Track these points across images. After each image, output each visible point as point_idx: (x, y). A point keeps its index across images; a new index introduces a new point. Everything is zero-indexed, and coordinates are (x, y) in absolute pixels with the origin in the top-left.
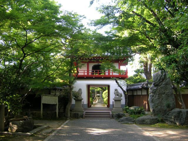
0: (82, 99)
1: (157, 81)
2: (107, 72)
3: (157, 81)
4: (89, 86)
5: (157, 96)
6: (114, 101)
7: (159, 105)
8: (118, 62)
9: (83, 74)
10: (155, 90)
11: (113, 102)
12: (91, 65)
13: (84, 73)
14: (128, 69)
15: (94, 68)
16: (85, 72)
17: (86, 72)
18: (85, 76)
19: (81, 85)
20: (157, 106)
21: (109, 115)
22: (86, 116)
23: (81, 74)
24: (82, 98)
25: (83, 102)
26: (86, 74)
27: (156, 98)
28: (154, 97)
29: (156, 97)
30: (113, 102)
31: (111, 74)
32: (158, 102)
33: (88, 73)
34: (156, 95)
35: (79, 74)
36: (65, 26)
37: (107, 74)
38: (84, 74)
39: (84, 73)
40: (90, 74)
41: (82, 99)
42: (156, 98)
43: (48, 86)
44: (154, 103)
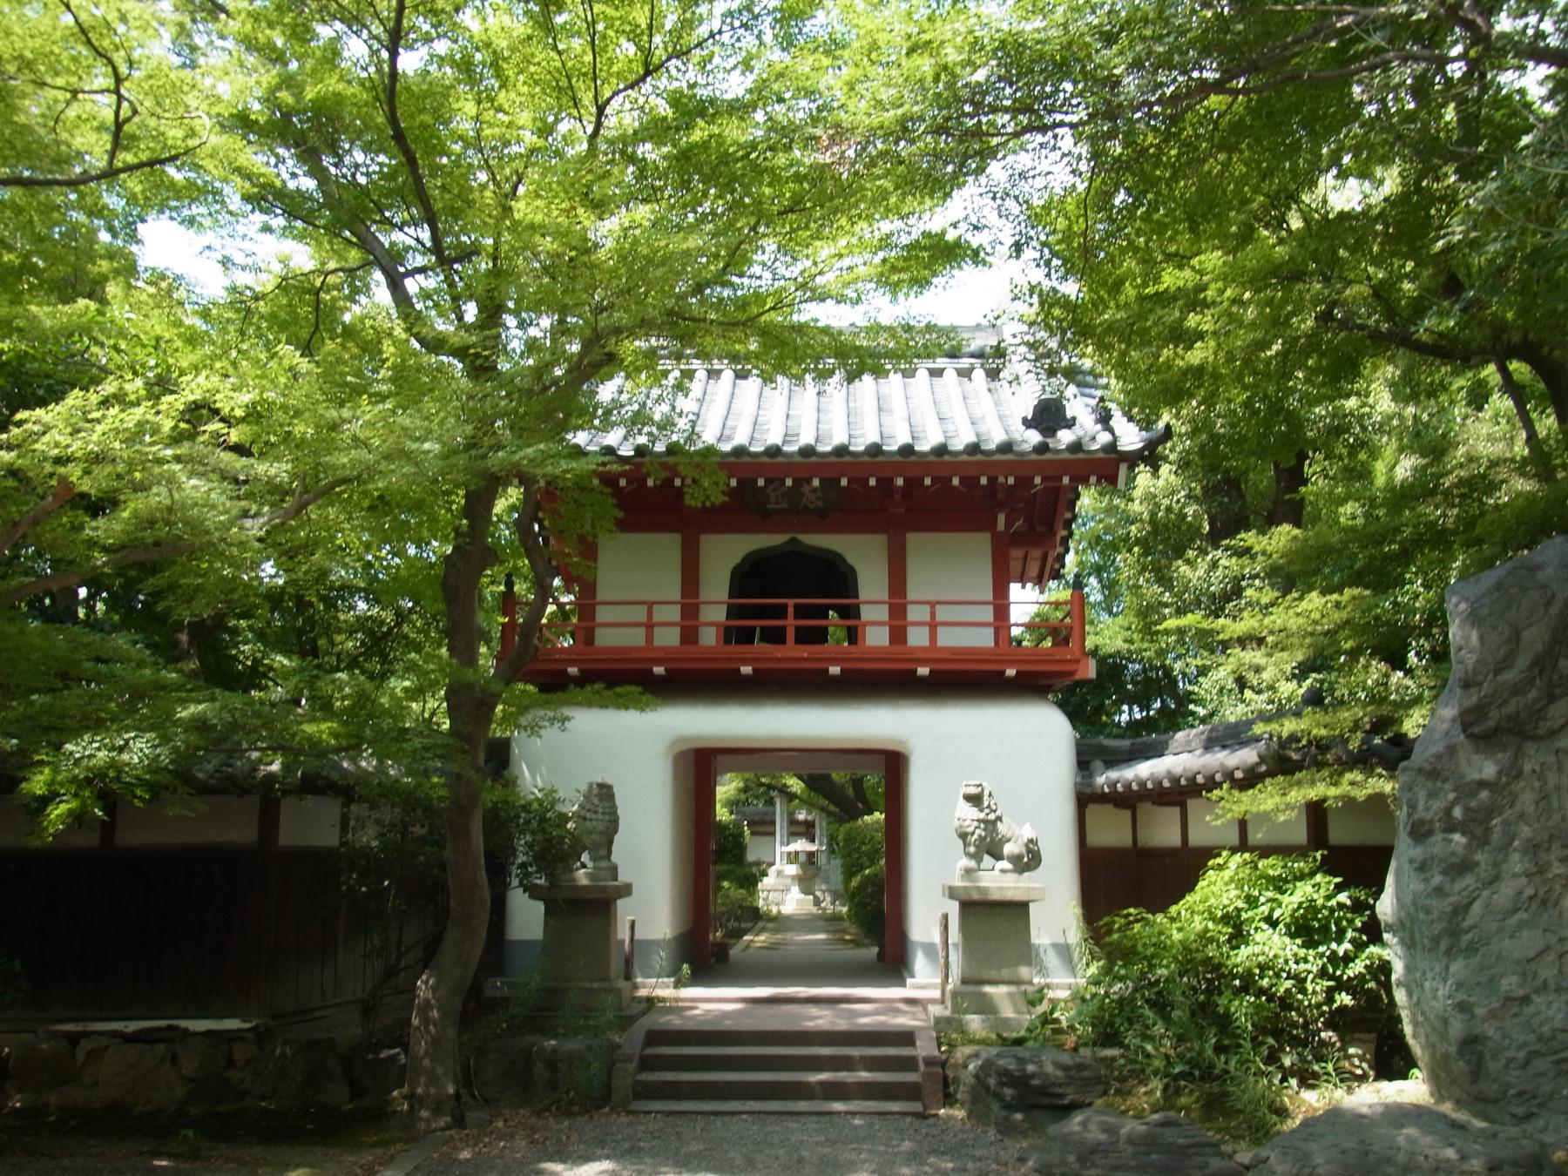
0: (626, 890)
1: (1508, 676)
2: (883, 613)
3: (1508, 676)
4: (699, 766)
5: (1517, 863)
6: (953, 909)
7: (1543, 989)
8: (990, 526)
9: (636, 638)
10: (1482, 784)
11: (946, 917)
12: (724, 554)
13: (650, 627)
14: (636, 953)
15: (752, 578)
16: (660, 614)
17: (674, 614)
18: (658, 662)
19: (613, 758)
20: (1526, 1000)
21: (909, 1064)
22: (645, 1076)
23: (617, 634)
24: (623, 877)
25: (633, 923)
26: (668, 638)
27: (1507, 889)
28: (1468, 880)
29: (1496, 879)
30: (946, 917)
31: (917, 638)
32: (1528, 943)
33: (689, 634)
34: (1505, 847)
35: (606, 638)
36: (531, 362)
37: (876, 637)
38: (650, 637)
39: (650, 627)
40: (709, 637)
41: (626, 890)
42: (1507, 889)
43: (334, 775)
44: (1471, 950)
